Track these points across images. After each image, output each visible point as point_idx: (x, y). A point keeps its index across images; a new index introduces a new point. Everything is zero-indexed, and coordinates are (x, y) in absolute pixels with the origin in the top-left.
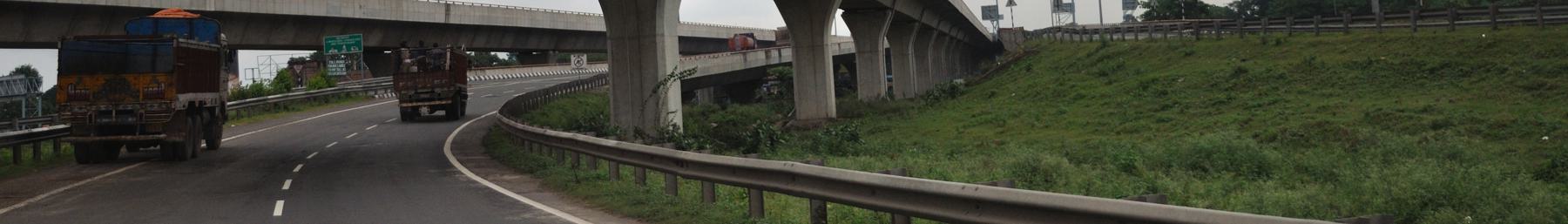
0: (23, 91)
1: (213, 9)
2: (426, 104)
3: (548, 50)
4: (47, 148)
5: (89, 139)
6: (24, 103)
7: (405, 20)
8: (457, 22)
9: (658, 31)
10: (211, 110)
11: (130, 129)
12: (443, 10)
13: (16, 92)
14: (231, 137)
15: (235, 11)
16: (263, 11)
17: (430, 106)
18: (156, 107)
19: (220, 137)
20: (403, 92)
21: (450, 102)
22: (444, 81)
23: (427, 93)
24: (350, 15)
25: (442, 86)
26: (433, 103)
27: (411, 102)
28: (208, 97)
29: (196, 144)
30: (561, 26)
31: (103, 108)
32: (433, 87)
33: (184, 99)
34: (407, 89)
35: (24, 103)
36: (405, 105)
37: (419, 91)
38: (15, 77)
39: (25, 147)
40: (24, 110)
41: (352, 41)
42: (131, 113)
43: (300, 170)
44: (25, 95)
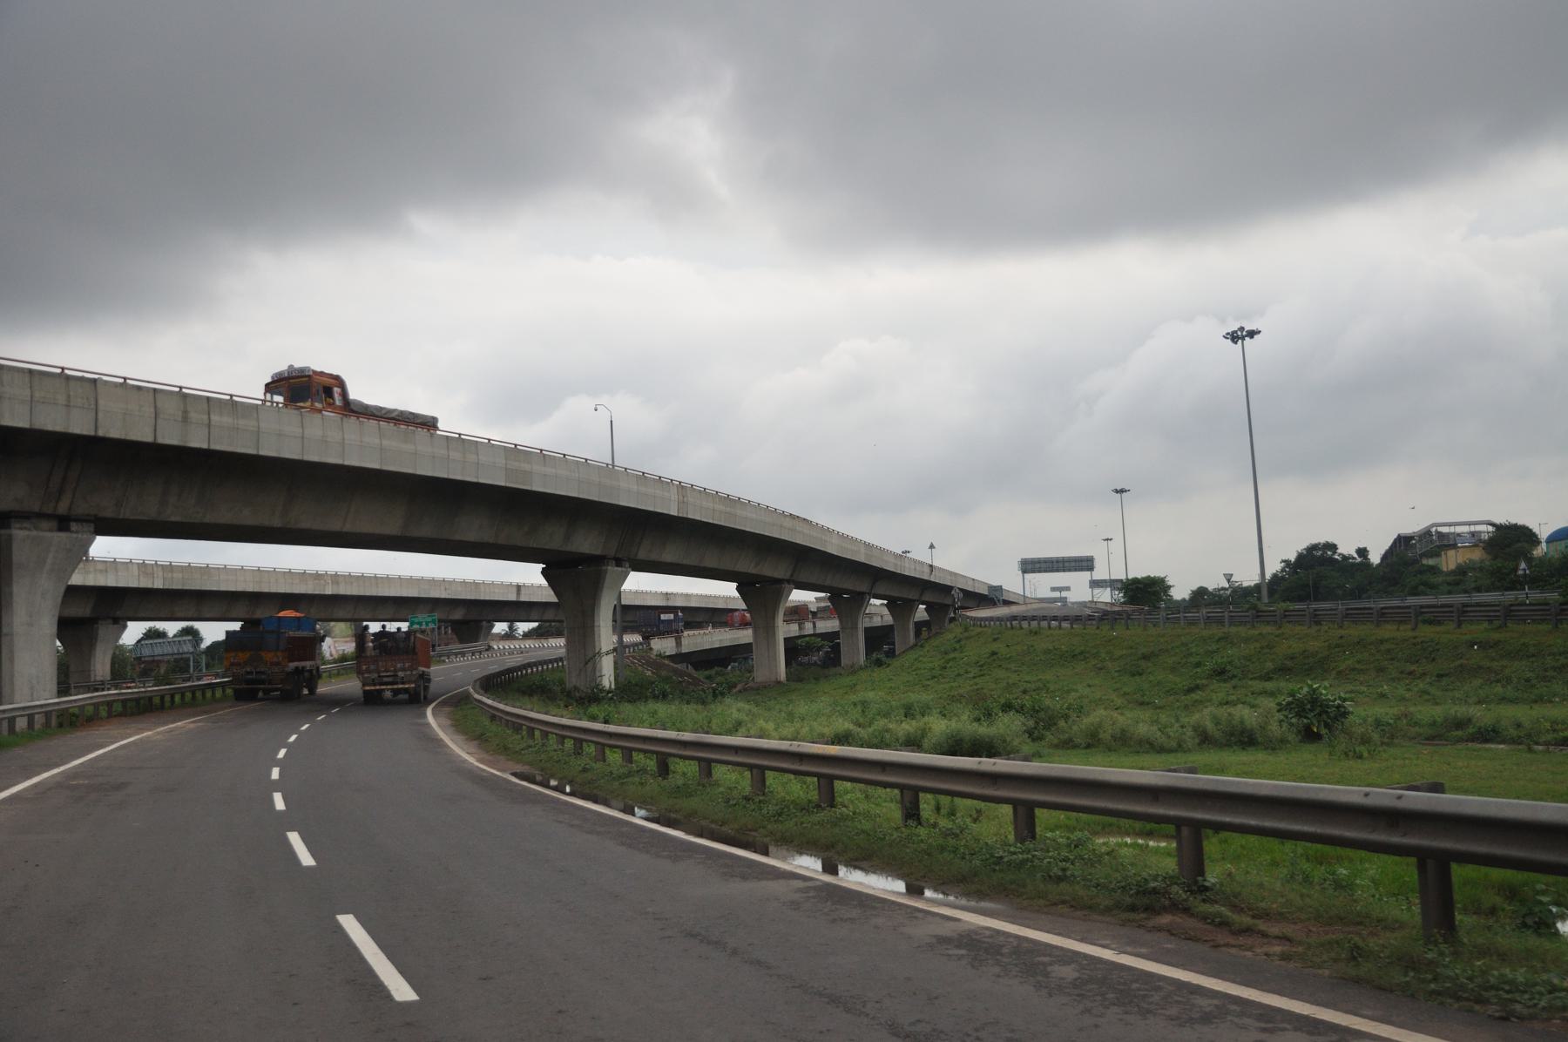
0: (191, 650)
1: (330, 593)
2: (389, 687)
4: (219, 693)
5: (241, 687)
6: (192, 659)
7: (482, 598)
8: (527, 600)
9: (596, 624)
10: (311, 671)
11: (263, 682)
12: (515, 590)
13: (186, 650)
14: (323, 689)
15: (391, 595)
16: (368, 594)
17: (392, 690)
18: (276, 670)
19: (316, 688)
20: (366, 675)
21: (413, 685)
22: (407, 665)
24: (437, 596)
25: (403, 670)
26: (395, 687)
27: (375, 685)
28: (308, 664)
29: (300, 690)
31: (249, 670)
32: (395, 671)
33: (293, 665)
34: (368, 671)
35: (192, 659)
37: (382, 674)
38: (176, 639)
39: (207, 690)
40: (192, 664)
41: (430, 619)
42: (263, 673)
43: (307, 729)
44: (192, 653)
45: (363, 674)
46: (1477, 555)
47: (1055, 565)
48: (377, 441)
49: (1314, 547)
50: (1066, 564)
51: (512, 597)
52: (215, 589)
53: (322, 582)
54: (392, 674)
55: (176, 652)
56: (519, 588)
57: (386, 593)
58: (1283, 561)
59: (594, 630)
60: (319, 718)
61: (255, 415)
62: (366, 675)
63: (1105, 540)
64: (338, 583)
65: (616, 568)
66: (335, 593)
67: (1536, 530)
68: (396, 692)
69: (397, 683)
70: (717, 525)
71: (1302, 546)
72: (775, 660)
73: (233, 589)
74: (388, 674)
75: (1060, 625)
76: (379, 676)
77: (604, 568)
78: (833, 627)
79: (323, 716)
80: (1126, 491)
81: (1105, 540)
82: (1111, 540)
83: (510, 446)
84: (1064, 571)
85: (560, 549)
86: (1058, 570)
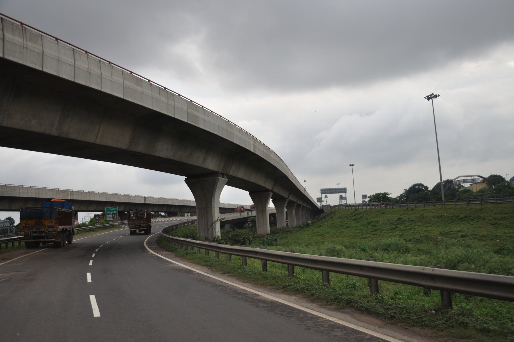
0: (9, 225)
1: (70, 199)
2: (138, 229)
3: (177, 212)
4: (16, 243)
10: (69, 231)
11: (43, 237)
13: (7, 225)
16: (86, 199)
20: (131, 225)
21: (146, 229)
22: (144, 222)
23: (138, 226)
25: (143, 223)
26: (140, 229)
27: (133, 228)
28: (68, 227)
30: (181, 204)
32: (140, 224)
33: (61, 227)
34: (132, 224)
36: (131, 230)
38: (6, 221)
40: (9, 231)
42: (43, 232)
44: (9, 226)
45: (130, 225)
46: (484, 186)
47: (335, 191)
48: (122, 81)
49: (416, 185)
50: (333, 191)
51: (143, 202)
52: (17, 196)
53: (66, 194)
54: (139, 225)
55: (2, 226)
56: (145, 198)
57: (93, 199)
58: (405, 190)
59: (212, 209)
60: (103, 245)
61: (40, 42)
62: (131, 225)
63: (337, 184)
64: (73, 195)
65: (222, 178)
66: (72, 199)
67: (504, 176)
68: (140, 231)
69: (141, 228)
70: (263, 158)
71: (411, 184)
72: (266, 222)
73: (26, 196)
74: (138, 225)
75: (376, 208)
76: (135, 226)
77: (217, 178)
78: (274, 212)
79: (107, 243)
80: (354, 165)
81: (337, 184)
82: (339, 184)
83: (12, 185)
84: (336, 193)
85: (201, 166)
86: (333, 193)
